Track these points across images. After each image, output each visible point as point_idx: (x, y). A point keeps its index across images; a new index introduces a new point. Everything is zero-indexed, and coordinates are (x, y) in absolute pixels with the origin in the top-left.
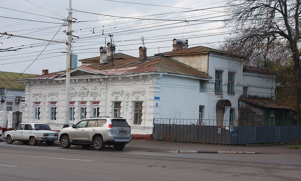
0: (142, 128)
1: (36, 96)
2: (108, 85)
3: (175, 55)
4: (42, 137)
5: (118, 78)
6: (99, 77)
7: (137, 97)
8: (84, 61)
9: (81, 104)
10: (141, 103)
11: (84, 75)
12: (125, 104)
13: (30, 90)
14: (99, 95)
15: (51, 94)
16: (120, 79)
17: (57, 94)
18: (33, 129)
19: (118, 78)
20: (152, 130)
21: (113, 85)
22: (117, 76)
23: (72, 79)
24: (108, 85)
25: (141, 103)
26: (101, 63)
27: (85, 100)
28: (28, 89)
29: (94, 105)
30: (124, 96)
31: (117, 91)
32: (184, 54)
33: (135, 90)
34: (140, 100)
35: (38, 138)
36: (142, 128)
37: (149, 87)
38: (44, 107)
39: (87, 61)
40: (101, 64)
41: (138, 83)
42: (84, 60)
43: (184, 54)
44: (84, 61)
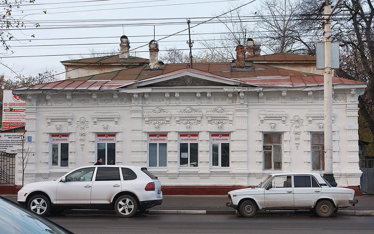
0: (232, 176)
1: (316, 121)
2: (249, 104)
3: (275, 62)
4: (352, 199)
5: (281, 92)
6: (239, 90)
7: (59, 126)
8: (76, 64)
9: (150, 136)
10: (279, 135)
11: (191, 85)
12: (293, 136)
13: (39, 110)
14: (230, 121)
15: (100, 119)
16: (284, 94)
17: (116, 120)
18: (321, 185)
19: (26, 95)
20: (358, 180)
21: (263, 104)
22: (280, 90)
23: (166, 91)
24: (249, 104)
25: (279, 135)
26: (152, 67)
27: (163, 129)
28: (35, 109)
29: (54, 140)
30: (289, 123)
31: (274, 115)
32: (293, 62)
33: (99, 115)
34: (278, 130)
35: (340, 202)
36: (232, 176)
37: (131, 111)
38: (82, 143)
39: (70, 64)
40: (151, 70)
41: (295, 102)
42: (77, 63)
43: (293, 62)
44: (76, 64)
